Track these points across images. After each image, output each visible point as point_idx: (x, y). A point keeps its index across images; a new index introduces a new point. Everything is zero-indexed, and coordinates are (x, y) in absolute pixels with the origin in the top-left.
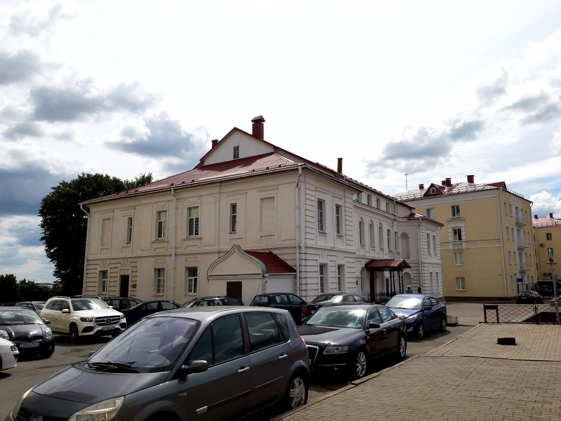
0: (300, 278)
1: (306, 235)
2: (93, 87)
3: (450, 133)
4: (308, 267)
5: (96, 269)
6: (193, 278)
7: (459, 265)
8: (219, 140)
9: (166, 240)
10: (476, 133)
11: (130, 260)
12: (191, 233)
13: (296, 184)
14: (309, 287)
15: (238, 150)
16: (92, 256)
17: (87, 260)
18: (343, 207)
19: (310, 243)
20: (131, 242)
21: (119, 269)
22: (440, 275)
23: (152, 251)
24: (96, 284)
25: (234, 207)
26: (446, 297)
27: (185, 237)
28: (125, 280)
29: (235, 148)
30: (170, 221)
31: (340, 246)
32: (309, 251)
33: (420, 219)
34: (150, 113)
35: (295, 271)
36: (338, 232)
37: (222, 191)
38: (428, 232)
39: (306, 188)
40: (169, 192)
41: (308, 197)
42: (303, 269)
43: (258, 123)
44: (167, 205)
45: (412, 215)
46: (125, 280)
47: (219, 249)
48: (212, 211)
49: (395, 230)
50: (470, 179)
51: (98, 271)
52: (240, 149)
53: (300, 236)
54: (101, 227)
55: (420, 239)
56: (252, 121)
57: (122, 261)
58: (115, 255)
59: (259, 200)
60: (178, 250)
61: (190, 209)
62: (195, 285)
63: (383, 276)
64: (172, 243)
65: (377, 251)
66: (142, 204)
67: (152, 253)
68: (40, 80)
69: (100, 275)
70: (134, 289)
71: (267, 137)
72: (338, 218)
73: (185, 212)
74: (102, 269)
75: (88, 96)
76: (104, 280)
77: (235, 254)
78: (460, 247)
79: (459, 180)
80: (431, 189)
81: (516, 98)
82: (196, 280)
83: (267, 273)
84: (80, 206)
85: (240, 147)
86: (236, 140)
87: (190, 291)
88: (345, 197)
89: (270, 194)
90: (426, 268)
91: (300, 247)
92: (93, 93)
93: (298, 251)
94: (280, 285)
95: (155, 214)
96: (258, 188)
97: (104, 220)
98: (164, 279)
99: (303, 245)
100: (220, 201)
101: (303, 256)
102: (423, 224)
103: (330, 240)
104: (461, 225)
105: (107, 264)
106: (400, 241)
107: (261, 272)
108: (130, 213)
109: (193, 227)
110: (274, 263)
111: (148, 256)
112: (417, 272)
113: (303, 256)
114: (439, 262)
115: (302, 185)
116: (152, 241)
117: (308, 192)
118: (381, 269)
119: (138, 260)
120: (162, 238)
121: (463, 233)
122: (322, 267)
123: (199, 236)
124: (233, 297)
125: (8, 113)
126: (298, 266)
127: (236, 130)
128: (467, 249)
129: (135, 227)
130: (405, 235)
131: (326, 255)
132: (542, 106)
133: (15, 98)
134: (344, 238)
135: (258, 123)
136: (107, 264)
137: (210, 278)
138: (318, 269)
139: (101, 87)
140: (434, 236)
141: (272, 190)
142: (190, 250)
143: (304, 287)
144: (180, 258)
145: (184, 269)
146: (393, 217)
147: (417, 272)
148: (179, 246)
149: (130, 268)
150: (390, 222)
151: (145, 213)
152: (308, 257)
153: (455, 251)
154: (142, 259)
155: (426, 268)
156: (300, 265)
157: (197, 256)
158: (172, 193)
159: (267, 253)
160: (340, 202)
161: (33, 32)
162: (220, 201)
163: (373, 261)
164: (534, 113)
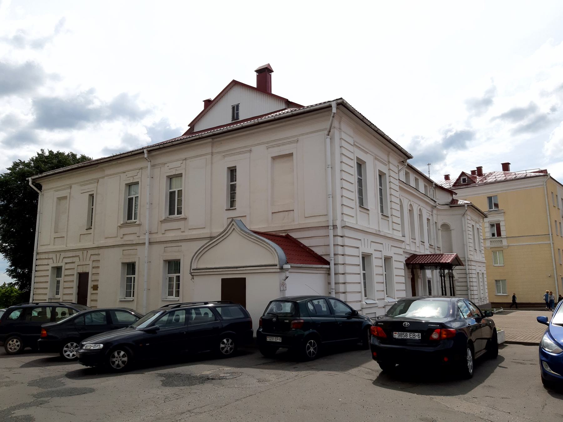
0: (335, 274)
1: (342, 209)
2: (95, 97)
3: (441, 142)
4: (347, 257)
5: (48, 265)
6: (174, 276)
7: (498, 265)
8: (212, 99)
9: (137, 223)
10: (468, 143)
11: (90, 252)
12: (171, 212)
13: (326, 132)
14: (349, 288)
15: (238, 110)
16: (44, 248)
17: (37, 253)
18: (387, 176)
19: (350, 222)
20: (92, 227)
21: (76, 264)
22: (485, 276)
23: (119, 239)
24: (47, 285)
25: (232, 171)
26: (492, 303)
27: (164, 218)
28: (83, 278)
29: (233, 108)
30: (143, 195)
31: (385, 230)
32: (347, 233)
33: (466, 205)
34: (148, 121)
35: (328, 263)
36: (382, 211)
37: (214, 151)
38: (474, 223)
39: (341, 139)
40: (141, 156)
41: (345, 152)
42: (340, 260)
43: (264, 74)
44: (139, 175)
45: (454, 202)
46: (83, 278)
47: (211, 233)
48: (202, 178)
49: (435, 220)
50: (506, 167)
51: (49, 268)
52: (240, 108)
53: (334, 209)
54: (55, 208)
55: (465, 231)
56: (256, 71)
57: (79, 253)
58: (72, 245)
59: (270, 159)
60: (154, 236)
61: (170, 178)
62: (178, 286)
63: (424, 275)
64: (146, 227)
65: (417, 244)
66: (108, 176)
67: (118, 241)
68: (43, 91)
69: (53, 273)
70: (95, 292)
71: (276, 90)
72: (381, 190)
73: (164, 182)
74: (55, 265)
75: (91, 107)
76: (58, 279)
77: (234, 234)
78: (498, 245)
79: (493, 169)
80: (462, 178)
81: (506, 109)
82: (178, 277)
83: (287, 263)
84: (28, 181)
85: (240, 105)
86: (235, 97)
87: (170, 294)
88: (389, 162)
89: (285, 150)
90: (473, 267)
91: (335, 227)
92: (96, 104)
93: (331, 233)
94: (304, 284)
95: (123, 187)
96: (267, 143)
97: (60, 199)
98: (134, 278)
99: (339, 224)
100: (212, 163)
101: (339, 241)
102: (468, 212)
103: (372, 221)
104: (500, 219)
105: (62, 257)
106: (440, 232)
107: (276, 262)
108: (91, 188)
109: (174, 203)
110: (297, 251)
111: (113, 246)
112: (463, 271)
113: (339, 241)
114: (484, 260)
115: (336, 134)
116: (119, 225)
117: (344, 144)
118: (423, 267)
119: (100, 251)
120: (133, 220)
121: (502, 228)
122: (366, 258)
123: (182, 216)
124: (231, 303)
125: (9, 121)
126: (332, 255)
127: (235, 83)
128: (508, 246)
129: (98, 208)
130: (446, 227)
131: (369, 242)
132: (532, 117)
133: (19, 108)
134: (390, 219)
135: (264, 74)
136: (62, 257)
137: (195, 273)
138: (359, 261)
139: (103, 97)
140: (478, 229)
141: (290, 143)
142: (171, 235)
143: (341, 288)
144: (156, 247)
145: (162, 263)
146: (432, 203)
147: (463, 271)
148: (154, 231)
149: (90, 263)
150: (429, 209)
151: (111, 191)
152: (347, 242)
153: (493, 250)
154: (106, 250)
155: (473, 267)
156: (335, 254)
157: (180, 244)
158: (146, 156)
159: (282, 237)
160: (384, 169)
161: (38, 45)
162: (212, 163)
163: (414, 256)
164: (524, 122)
